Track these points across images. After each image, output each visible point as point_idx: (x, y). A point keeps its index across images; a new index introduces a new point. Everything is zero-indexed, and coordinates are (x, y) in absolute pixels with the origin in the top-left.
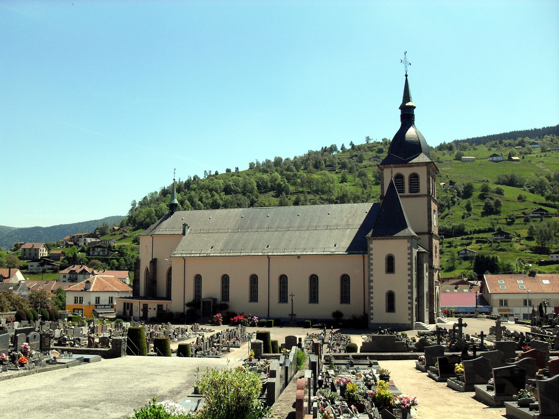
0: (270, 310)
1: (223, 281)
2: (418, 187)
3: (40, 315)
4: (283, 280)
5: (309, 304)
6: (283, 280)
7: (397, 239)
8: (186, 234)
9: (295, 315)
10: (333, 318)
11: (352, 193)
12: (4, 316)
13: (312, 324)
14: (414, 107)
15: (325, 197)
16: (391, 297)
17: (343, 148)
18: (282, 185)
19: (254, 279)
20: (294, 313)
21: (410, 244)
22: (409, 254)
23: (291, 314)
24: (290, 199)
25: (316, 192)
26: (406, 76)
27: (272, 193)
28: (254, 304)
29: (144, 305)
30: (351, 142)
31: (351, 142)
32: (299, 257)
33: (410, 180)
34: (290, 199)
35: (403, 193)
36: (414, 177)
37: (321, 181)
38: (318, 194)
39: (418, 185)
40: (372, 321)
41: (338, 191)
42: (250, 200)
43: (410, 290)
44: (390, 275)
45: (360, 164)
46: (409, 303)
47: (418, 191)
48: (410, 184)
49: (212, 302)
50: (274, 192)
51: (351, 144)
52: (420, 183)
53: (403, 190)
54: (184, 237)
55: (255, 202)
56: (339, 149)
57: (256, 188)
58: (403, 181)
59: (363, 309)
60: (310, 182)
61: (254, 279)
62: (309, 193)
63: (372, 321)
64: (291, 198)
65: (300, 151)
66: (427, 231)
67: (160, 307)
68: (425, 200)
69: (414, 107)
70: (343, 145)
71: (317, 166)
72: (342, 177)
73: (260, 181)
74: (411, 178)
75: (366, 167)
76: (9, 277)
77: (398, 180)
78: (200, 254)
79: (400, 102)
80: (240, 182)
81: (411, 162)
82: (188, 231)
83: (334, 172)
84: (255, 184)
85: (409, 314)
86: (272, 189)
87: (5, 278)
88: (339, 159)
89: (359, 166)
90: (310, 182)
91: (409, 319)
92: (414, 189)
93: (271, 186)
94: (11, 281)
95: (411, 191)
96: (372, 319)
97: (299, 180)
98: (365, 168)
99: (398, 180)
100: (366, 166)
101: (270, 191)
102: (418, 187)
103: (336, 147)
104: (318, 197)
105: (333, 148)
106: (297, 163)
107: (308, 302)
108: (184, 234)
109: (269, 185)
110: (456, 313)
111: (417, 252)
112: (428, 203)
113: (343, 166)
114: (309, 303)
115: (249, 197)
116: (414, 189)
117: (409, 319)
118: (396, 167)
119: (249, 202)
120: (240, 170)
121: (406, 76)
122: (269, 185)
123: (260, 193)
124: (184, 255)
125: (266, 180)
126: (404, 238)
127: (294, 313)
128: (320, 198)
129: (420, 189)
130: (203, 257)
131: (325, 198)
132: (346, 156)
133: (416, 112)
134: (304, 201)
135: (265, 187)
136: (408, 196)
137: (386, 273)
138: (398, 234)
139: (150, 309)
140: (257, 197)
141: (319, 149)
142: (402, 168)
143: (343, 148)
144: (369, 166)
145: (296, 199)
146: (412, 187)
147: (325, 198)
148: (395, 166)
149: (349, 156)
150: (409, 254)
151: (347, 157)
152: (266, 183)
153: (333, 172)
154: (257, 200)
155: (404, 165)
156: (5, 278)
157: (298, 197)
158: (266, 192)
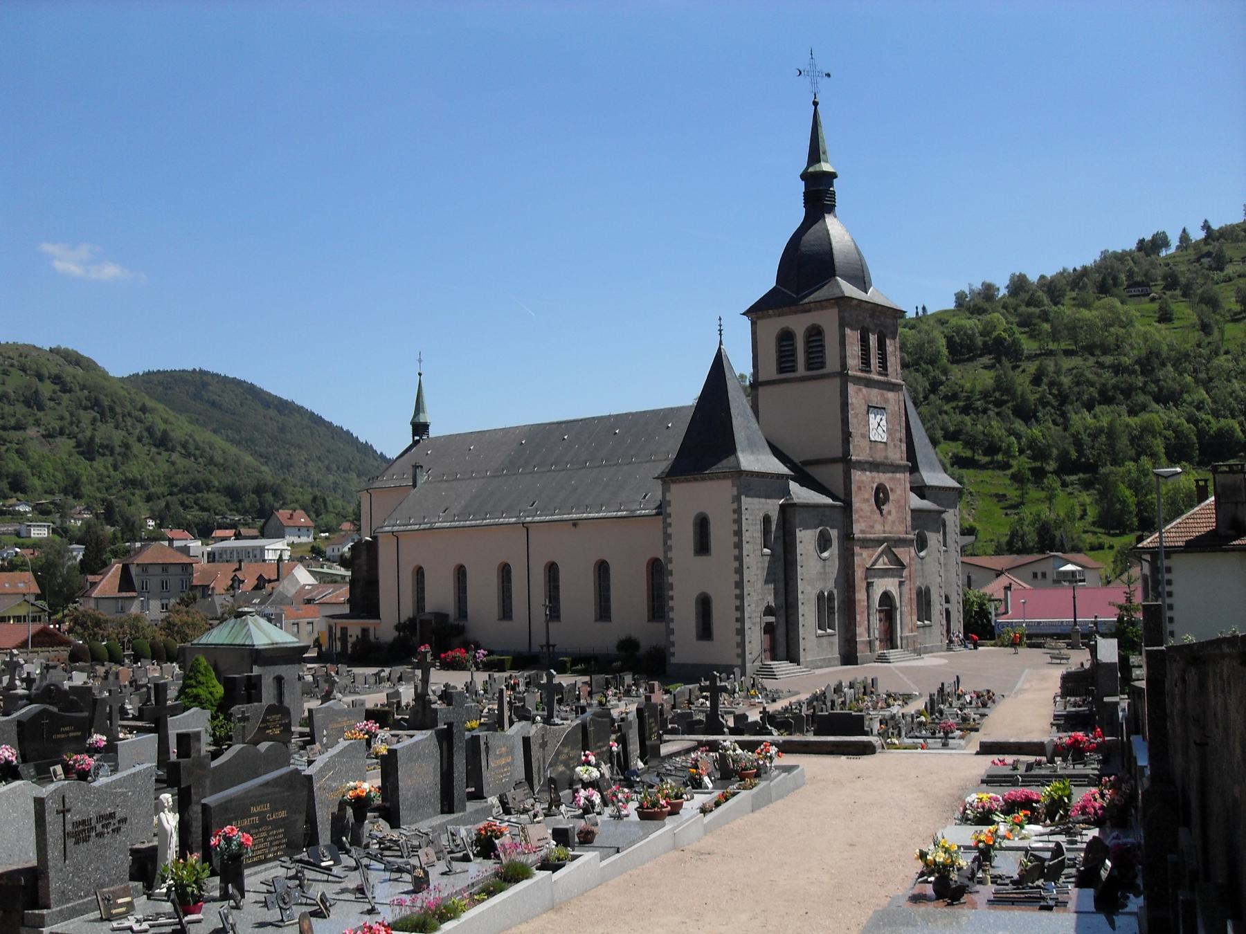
0: (532, 635)
1: (459, 578)
2: (822, 357)
3: (130, 652)
4: (552, 570)
5: (597, 623)
6: (552, 570)
7: (711, 479)
8: (419, 484)
9: (554, 646)
10: (617, 653)
11: (1171, 348)
12: (42, 654)
13: (572, 666)
14: (832, 176)
15: (1108, 360)
16: (704, 604)
17: (1184, 237)
18: (1005, 339)
19: (505, 572)
20: (551, 643)
21: (738, 489)
22: (734, 511)
23: (545, 643)
24: (1024, 371)
25: (1090, 349)
26: (815, 104)
27: (986, 360)
28: (506, 624)
29: (342, 628)
30: (1206, 221)
31: (1206, 221)
32: (575, 525)
33: (807, 342)
34: (1024, 371)
35: (794, 371)
36: (815, 334)
37: (1100, 324)
38: (1093, 355)
39: (821, 351)
40: (673, 660)
41: (1139, 344)
42: (928, 379)
43: (737, 592)
44: (703, 559)
45: (1216, 275)
46: (737, 620)
47: (822, 365)
48: (808, 352)
49: (433, 622)
50: (991, 357)
51: (1206, 226)
52: (826, 348)
53: (794, 366)
54: (413, 491)
55: (942, 383)
56: (1174, 242)
57: (945, 351)
58: (793, 345)
59: (545, 634)
60: (1073, 330)
61: (505, 572)
62: (1068, 353)
63: (673, 660)
64: (1027, 369)
65: (1084, 256)
66: (841, 455)
67: (365, 631)
68: (836, 382)
69: (832, 176)
70: (1184, 230)
71: (1103, 289)
72: (1161, 308)
73: (958, 334)
74: (810, 336)
75: (1230, 279)
76: (278, 580)
77: (785, 343)
78: (420, 525)
79: (802, 163)
80: (908, 340)
81: (806, 300)
82: (422, 479)
83: (1147, 299)
84: (943, 342)
85: (737, 643)
86: (987, 349)
87: (270, 581)
88: (1167, 265)
89: (1213, 279)
90: (1074, 328)
91: (738, 656)
92: (816, 360)
93: (985, 343)
94: (281, 586)
95: (809, 367)
96: (673, 654)
97: (1046, 326)
98: (1226, 282)
99: (785, 343)
100: (1229, 278)
101: (981, 355)
102: (822, 357)
103: (1166, 237)
104: (1092, 360)
105: (1159, 241)
106: (1055, 287)
107: (647, 619)
108: (414, 486)
109: (979, 341)
110: (1029, 636)
111: (781, 506)
112: (841, 391)
113: (1171, 282)
114: (500, 619)
115: (925, 373)
116: (816, 360)
117: (738, 656)
118: (779, 316)
119: (927, 385)
120: (929, 312)
121: (815, 104)
122: (979, 341)
123: (952, 363)
124: (396, 528)
125: (970, 332)
126: (725, 478)
127: (551, 643)
128: (1097, 362)
129: (827, 363)
130: (615, 520)
131: (1107, 364)
132: (1187, 258)
133: (837, 185)
134: (1055, 373)
135: (971, 348)
136: (802, 379)
137: (695, 555)
138: (714, 469)
139: (351, 636)
140: (945, 372)
141: (1131, 245)
142: (791, 316)
143: (1184, 237)
144: (1239, 276)
145: (1036, 370)
146: (813, 358)
147: (1107, 364)
148: (776, 312)
149: (1193, 257)
150: (734, 511)
151: (1189, 260)
152: (971, 338)
153: (1143, 298)
154: (947, 379)
155: (793, 308)
156: (270, 581)
157: (1041, 364)
158: (971, 359)
